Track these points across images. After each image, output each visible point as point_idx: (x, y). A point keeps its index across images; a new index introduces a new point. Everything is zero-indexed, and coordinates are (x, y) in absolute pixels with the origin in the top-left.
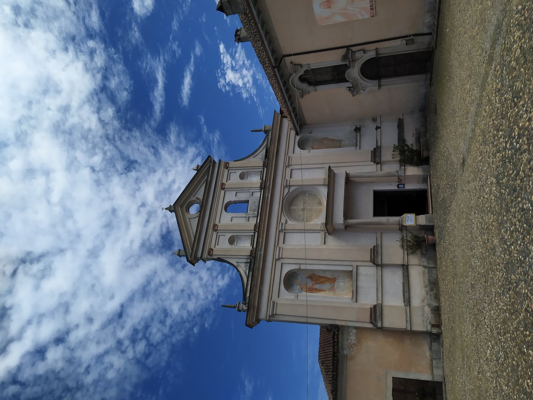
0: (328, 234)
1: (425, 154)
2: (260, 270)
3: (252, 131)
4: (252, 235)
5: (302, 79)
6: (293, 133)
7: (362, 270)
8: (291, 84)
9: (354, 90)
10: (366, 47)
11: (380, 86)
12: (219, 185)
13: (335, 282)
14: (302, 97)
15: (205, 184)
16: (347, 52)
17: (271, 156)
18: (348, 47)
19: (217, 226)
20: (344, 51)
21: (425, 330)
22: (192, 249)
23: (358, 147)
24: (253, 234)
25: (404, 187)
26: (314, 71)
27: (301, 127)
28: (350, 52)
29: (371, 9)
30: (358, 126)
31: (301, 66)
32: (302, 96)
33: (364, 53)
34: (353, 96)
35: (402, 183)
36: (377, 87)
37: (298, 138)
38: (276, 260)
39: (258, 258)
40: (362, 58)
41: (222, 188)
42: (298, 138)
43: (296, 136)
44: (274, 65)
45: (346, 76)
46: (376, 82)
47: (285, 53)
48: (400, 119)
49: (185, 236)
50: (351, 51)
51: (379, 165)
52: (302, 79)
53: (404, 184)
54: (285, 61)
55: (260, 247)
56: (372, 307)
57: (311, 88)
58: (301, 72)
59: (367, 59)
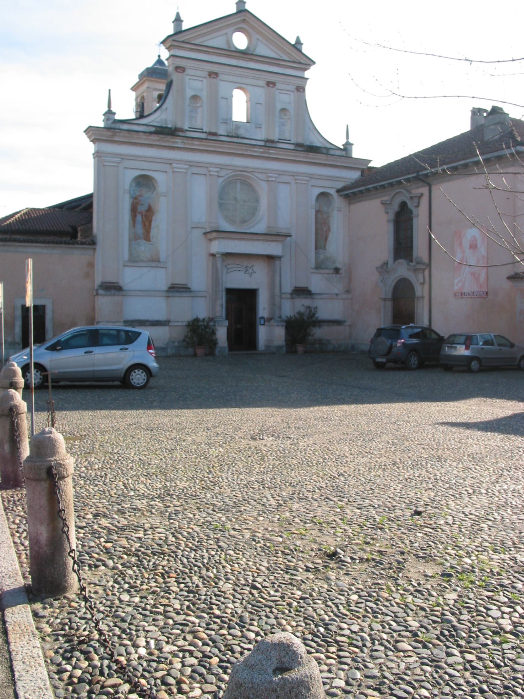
0: (204, 232)
1: (300, 348)
2: (158, 143)
3: (110, 90)
4: (202, 129)
5: (403, 205)
6: (340, 185)
7: (162, 272)
8: (397, 191)
9: (384, 268)
10: (426, 286)
11: (385, 299)
12: (274, 79)
13: (146, 240)
14: (382, 204)
15: (254, 173)
16: (424, 264)
17: (312, 155)
18: (429, 265)
19: (215, 76)
20: (426, 260)
21: (416, 295)
22: (183, 42)
23: (314, 271)
24: (204, 130)
25: (261, 324)
26: (410, 220)
27: (347, 196)
28: (424, 267)
29: (462, 293)
30: (341, 271)
31: (418, 206)
32: (383, 203)
33: (421, 283)
34: (377, 268)
35: (266, 323)
36: (384, 297)
37: (333, 192)
38: (171, 164)
39: (173, 140)
40: (416, 280)
41: (268, 83)
42: (333, 192)
43: (335, 190)
44: (420, 173)
45: (400, 260)
46: (390, 295)
47: (434, 188)
48: (345, 321)
49: (201, 30)
50: (425, 269)
51: (289, 296)
52: (403, 205)
53: (264, 324)
54: (423, 186)
55: (186, 142)
56: (206, 319)
57: (392, 216)
58: (410, 205)
59: (414, 284)
